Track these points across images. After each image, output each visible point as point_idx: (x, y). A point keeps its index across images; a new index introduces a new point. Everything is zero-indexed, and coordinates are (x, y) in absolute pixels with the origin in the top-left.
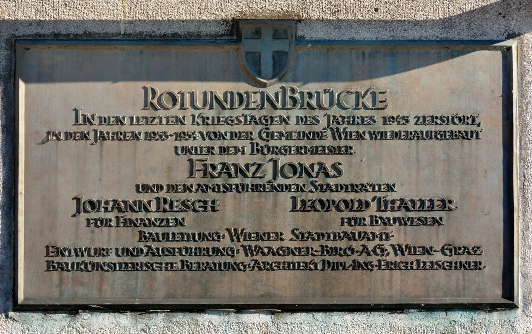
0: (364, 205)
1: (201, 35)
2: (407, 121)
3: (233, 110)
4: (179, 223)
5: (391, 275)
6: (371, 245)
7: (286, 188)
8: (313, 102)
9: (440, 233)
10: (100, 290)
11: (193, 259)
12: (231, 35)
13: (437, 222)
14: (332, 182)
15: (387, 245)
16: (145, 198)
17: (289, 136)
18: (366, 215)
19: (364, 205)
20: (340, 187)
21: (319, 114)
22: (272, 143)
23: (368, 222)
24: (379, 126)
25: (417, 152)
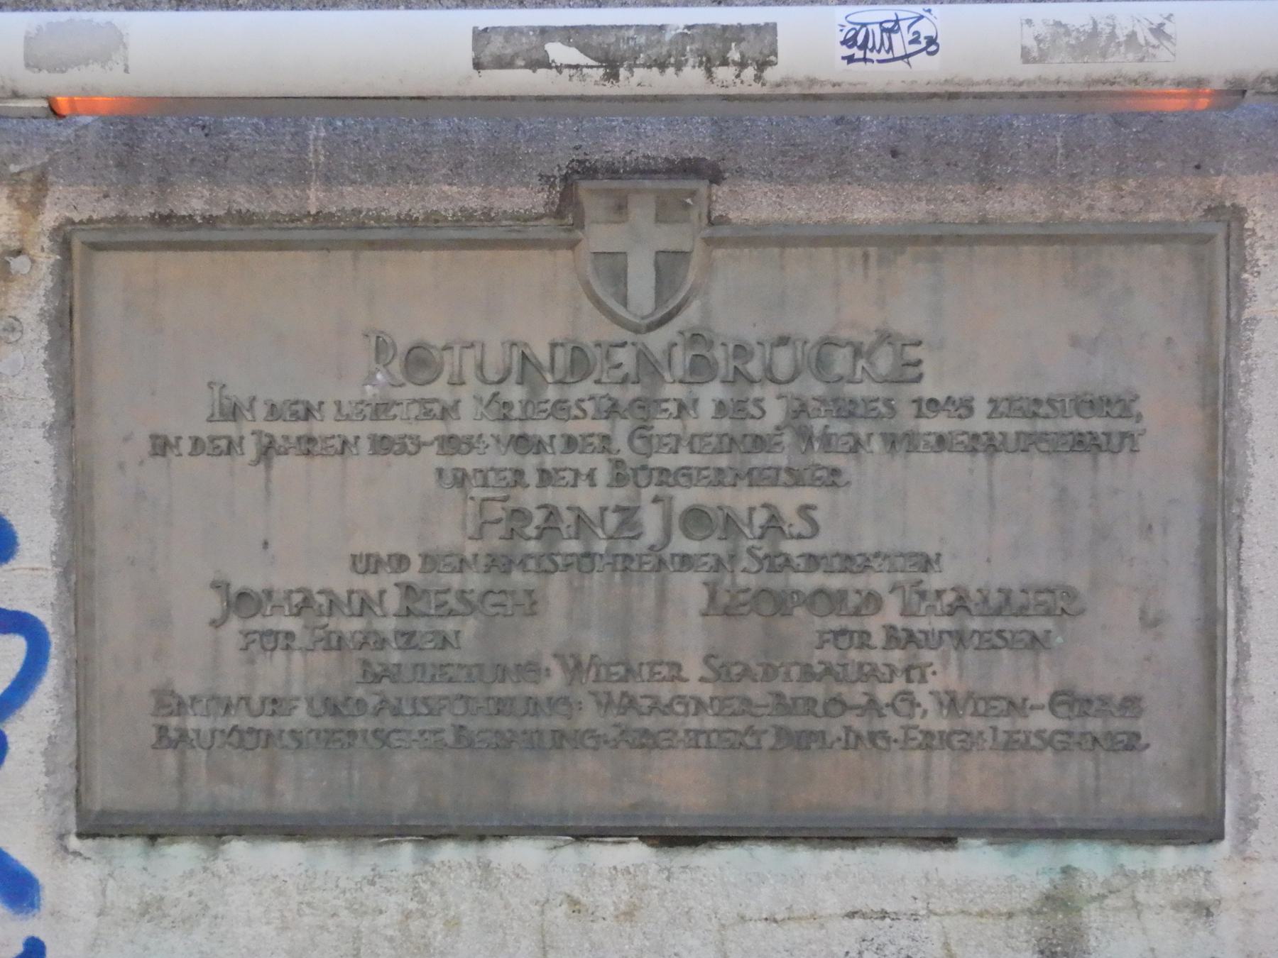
0: (873, 601)
1: (493, 215)
2: (971, 410)
3: (566, 386)
4: (444, 642)
5: (928, 764)
6: (884, 693)
7: (686, 561)
8: (754, 368)
9: (1043, 667)
10: (270, 791)
11: (475, 724)
12: (559, 214)
13: (1036, 642)
14: (792, 548)
15: (921, 693)
16: (370, 584)
17: (694, 443)
18: (874, 625)
19: (873, 601)
20: (813, 561)
21: (768, 393)
22: (658, 460)
23: (878, 638)
24: (906, 420)
25: (991, 484)
